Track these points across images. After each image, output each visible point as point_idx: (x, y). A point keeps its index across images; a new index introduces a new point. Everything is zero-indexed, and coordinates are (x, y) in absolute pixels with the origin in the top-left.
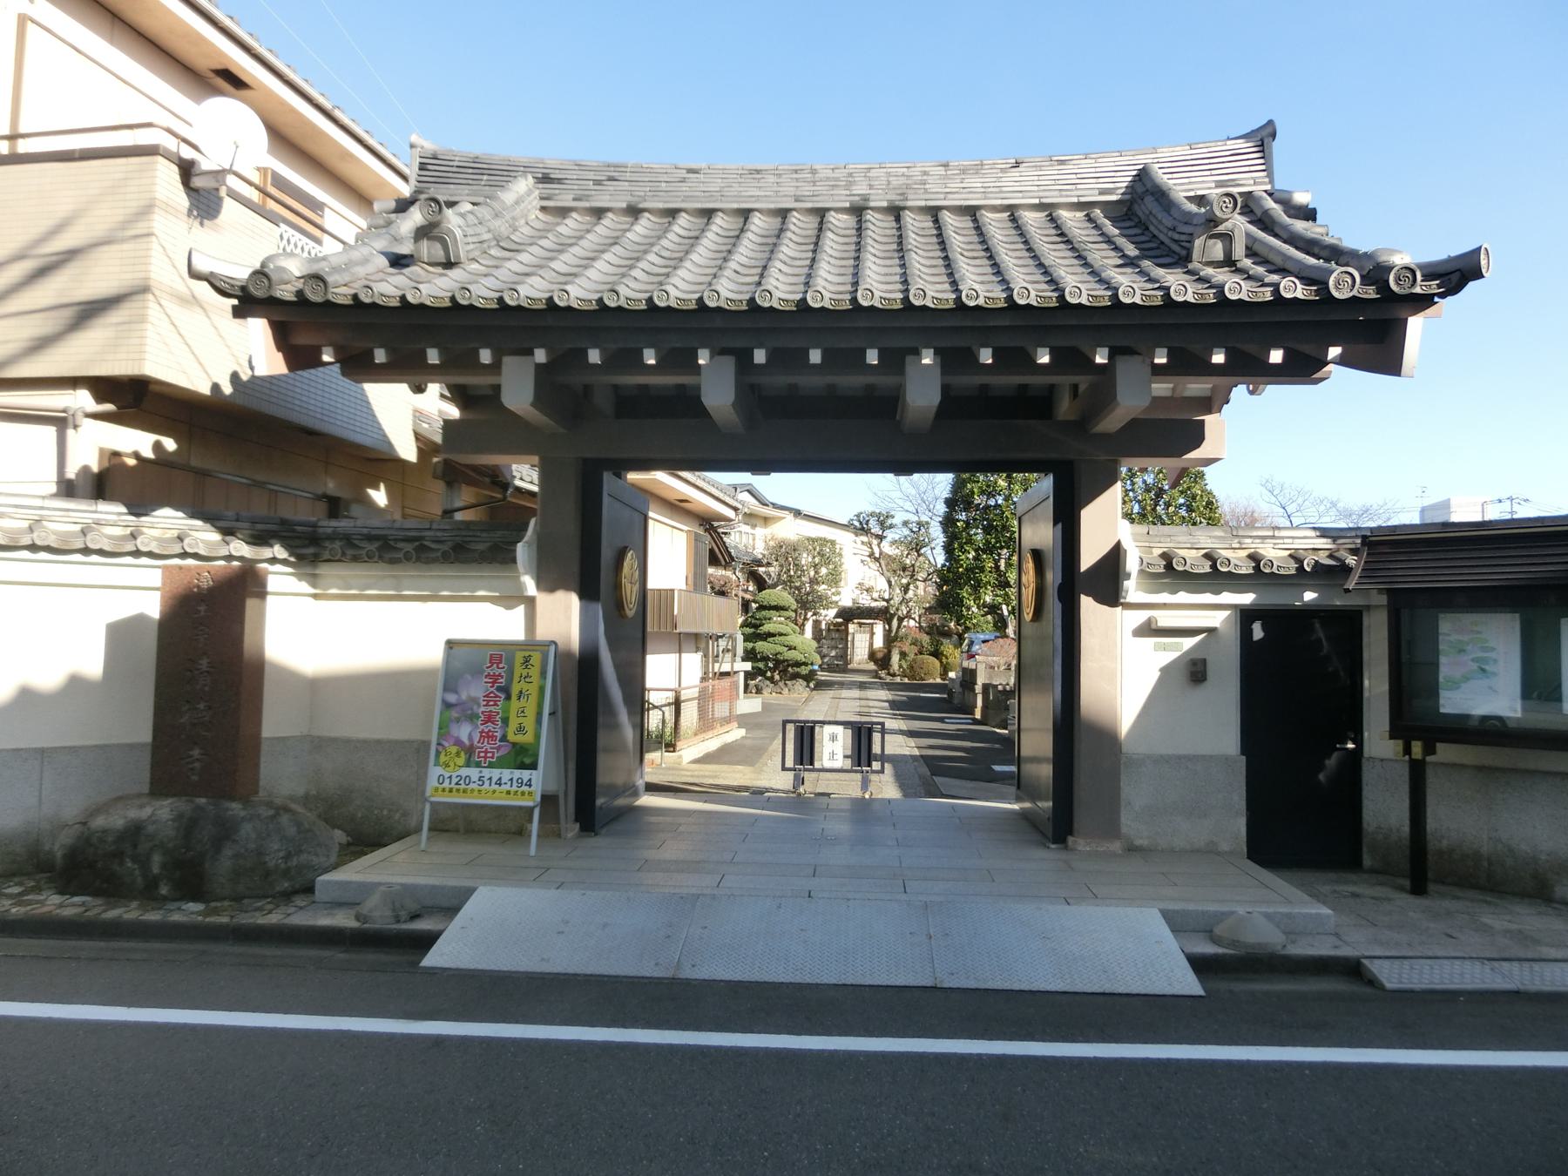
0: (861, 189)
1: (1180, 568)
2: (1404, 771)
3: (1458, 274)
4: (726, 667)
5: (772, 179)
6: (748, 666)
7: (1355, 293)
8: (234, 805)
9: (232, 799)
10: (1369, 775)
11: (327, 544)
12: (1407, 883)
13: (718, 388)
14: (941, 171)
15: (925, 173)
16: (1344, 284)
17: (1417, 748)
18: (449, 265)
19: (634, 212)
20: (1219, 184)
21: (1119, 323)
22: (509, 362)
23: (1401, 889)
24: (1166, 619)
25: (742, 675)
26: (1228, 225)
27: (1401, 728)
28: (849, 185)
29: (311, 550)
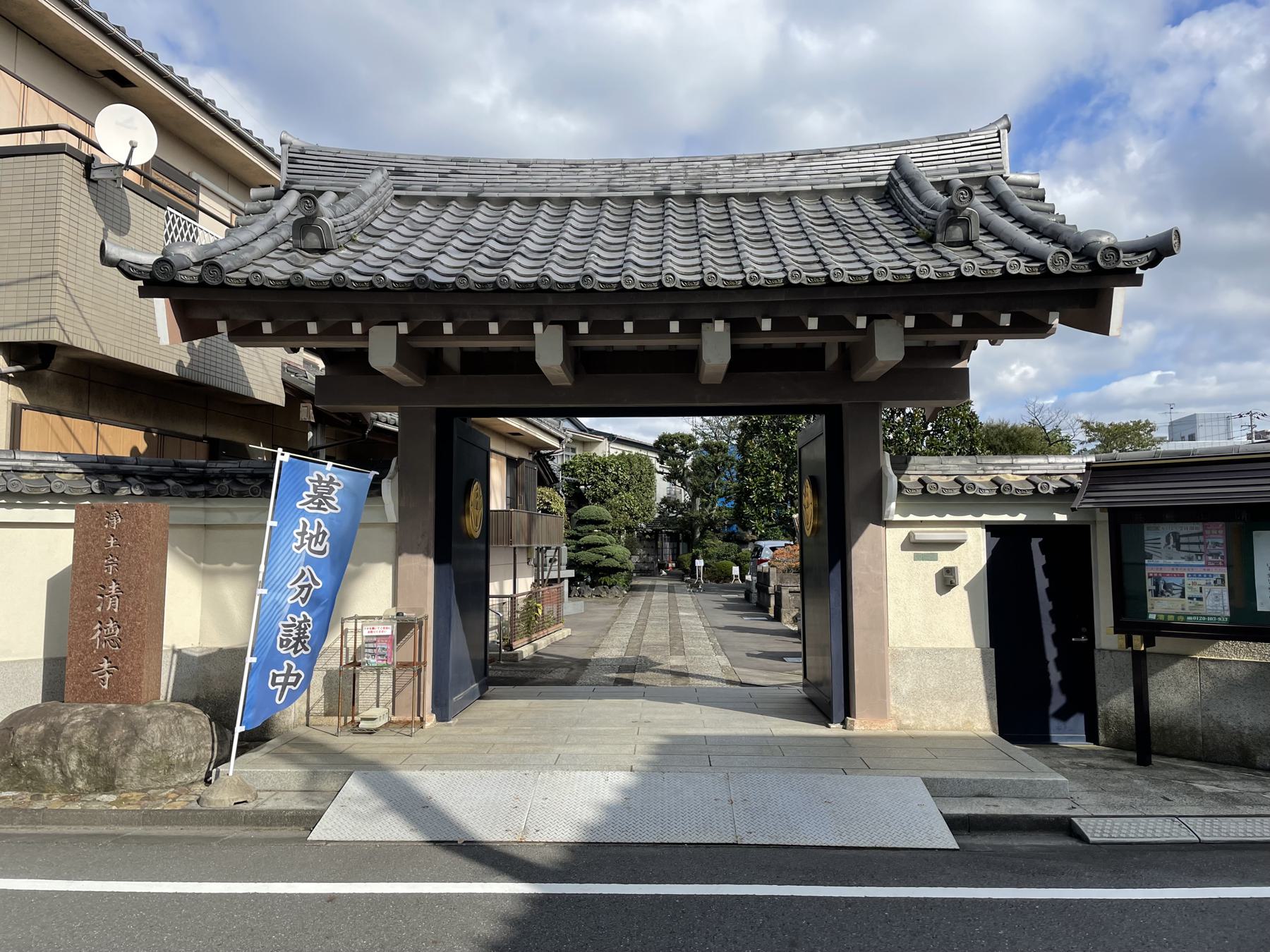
0: (662, 180)
1: (933, 492)
2: (1128, 659)
3: (1160, 250)
4: (554, 575)
5: (589, 172)
6: (571, 573)
7: (1069, 268)
8: (140, 709)
9: (138, 704)
10: (1100, 664)
11: (215, 483)
12: (1134, 756)
13: (549, 349)
14: (729, 164)
15: (716, 166)
16: (1059, 262)
17: (1137, 639)
18: (324, 251)
19: (475, 200)
20: (962, 171)
21: (876, 296)
22: (375, 331)
23: (1130, 761)
24: (923, 534)
25: (566, 582)
26: (966, 212)
27: (1120, 626)
28: (655, 175)
29: (201, 488)
